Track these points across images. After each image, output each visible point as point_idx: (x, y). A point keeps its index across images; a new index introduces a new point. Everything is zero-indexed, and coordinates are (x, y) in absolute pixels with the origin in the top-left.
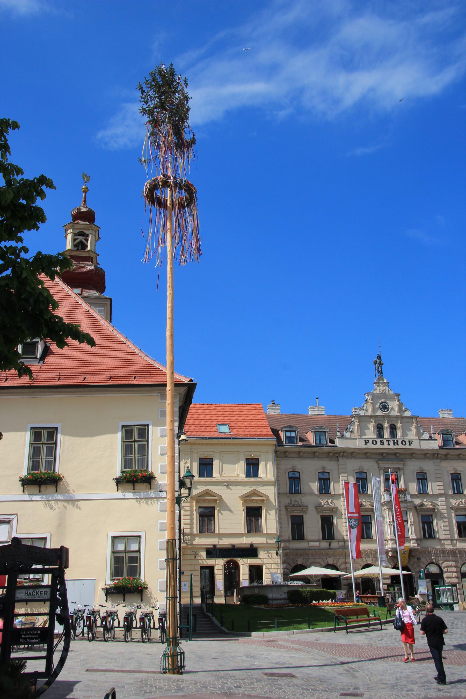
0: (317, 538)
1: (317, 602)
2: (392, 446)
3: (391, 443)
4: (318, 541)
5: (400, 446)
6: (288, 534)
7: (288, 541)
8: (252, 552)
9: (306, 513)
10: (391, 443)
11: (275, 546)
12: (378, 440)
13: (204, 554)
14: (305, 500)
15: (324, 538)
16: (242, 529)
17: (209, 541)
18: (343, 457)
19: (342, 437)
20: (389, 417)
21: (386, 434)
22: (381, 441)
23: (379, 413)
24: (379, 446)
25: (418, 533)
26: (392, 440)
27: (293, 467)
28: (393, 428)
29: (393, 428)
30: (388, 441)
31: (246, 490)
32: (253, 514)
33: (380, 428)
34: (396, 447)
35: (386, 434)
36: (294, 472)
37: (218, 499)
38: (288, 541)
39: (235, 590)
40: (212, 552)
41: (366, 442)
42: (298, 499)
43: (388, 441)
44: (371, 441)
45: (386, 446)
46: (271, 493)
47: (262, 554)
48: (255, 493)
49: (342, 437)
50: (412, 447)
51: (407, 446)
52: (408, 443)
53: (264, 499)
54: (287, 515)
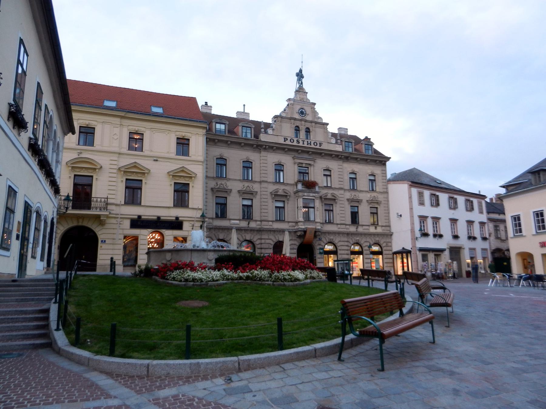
0: (238, 218)
1: (342, 282)
2: (305, 145)
3: (306, 143)
4: (239, 220)
5: (313, 146)
6: (212, 212)
7: (212, 219)
8: (177, 224)
9: (229, 195)
10: (306, 143)
11: (200, 219)
12: (295, 139)
13: (127, 223)
14: (230, 185)
15: (244, 218)
16: (170, 202)
17: (134, 211)
18: (265, 149)
19: (266, 132)
20: (306, 121)
21: (302, 134)
22: (297, 141)
23: (297, 116)
24: (295, 143)
25: (321, 218)
26: (306, 140)
27: (220, 155)
28: (308, 131)
29: (308, 131)
30: (303, 141)
31: (174, 166)
32: (181, 194)
33: (297, 129)
34: (309, 146)
35: (302, 134)
36: (221, 158)
37: (145, 172)
38: (212, 219)
39: (71, 245)
40: (138, 223)
41: (285, 139)
42: (223, 183)
43: (303, 141)
44: (289, 139)
45: (301, 144)
46: (199, 170)
47: (186, 225)
48: (183, 170)
49: (266, 132)
50: (322, 147)
51: (318, 147)
52: (318, 145)
53: (191, 176)
54: (213, 196)
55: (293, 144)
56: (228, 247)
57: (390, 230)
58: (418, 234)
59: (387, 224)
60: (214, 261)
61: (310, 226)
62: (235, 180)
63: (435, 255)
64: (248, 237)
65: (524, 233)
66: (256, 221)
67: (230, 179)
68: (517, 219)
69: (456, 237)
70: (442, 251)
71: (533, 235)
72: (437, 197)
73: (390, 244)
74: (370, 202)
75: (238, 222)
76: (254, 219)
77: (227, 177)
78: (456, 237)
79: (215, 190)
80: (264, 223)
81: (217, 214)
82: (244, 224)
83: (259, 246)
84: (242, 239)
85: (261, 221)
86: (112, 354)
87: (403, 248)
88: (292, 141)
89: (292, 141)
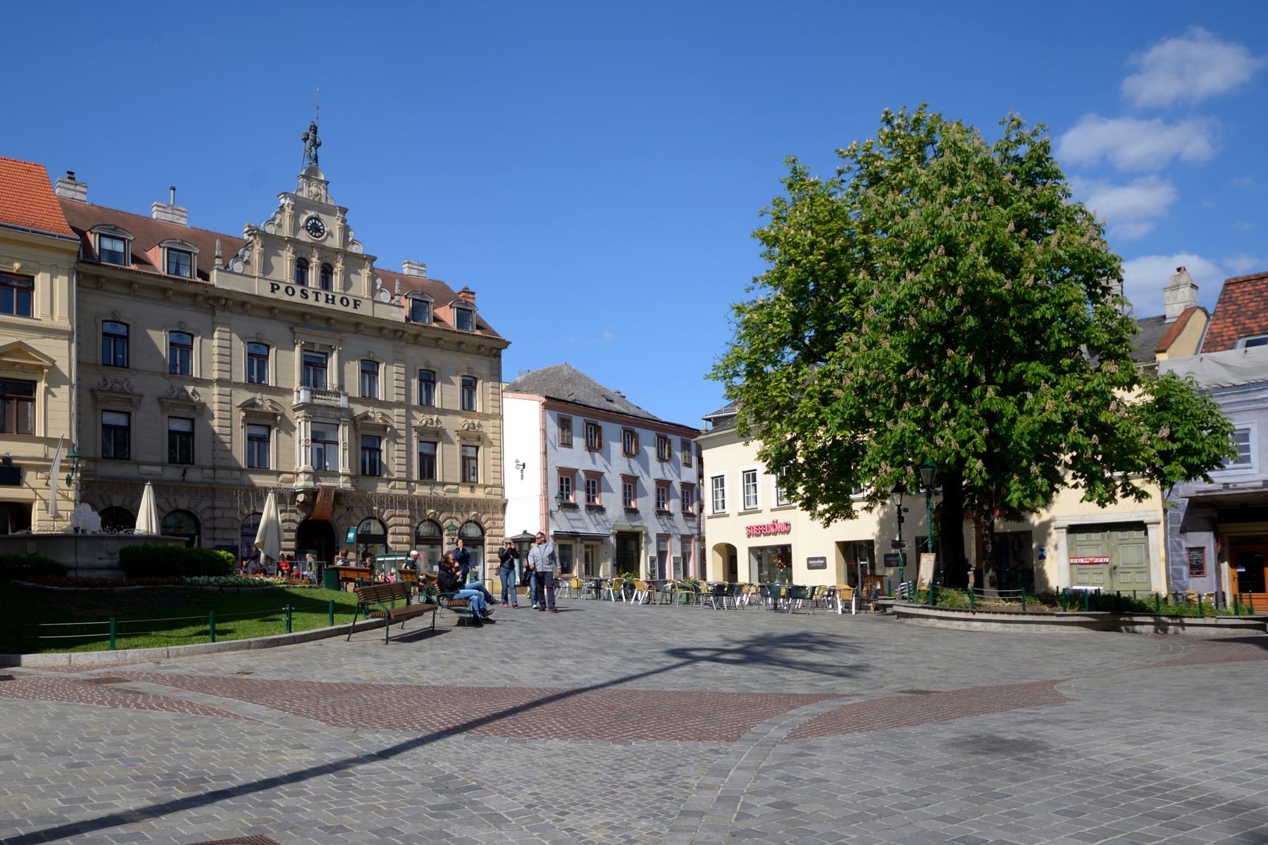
0: (158, 459)
2: (322, 303)
3: (322, 298)
4: (162, 465)
5: (338, 306)
10: (322, 298)
14: (137, 383)
15: (172, 460)
22: (302, 291)
24: (297, 298)
26: (323, 293)
27: (113, 313)
34: (330, 306)
41: (274, 287)
44: (283, 287)
45: (311, 301)
47: (30, 477)
51: (350, 309)
52: (352, 303)
55: (293, 299)
56: (716, 672)
57: (502, 495)
58: (554, 505)
59: (498, 482)
60: (117, 556)
61: (326, 483)
62: (152, 373)
63: (587, 546)
64: (183, 504)
65: (727, 510)
66: (202, 468)
67: (138, 371)
68: (719, 481)
69: (632, 512)
70: (600, 539)
71: (740, 514)
72: (598, 429)
73: (500, 523)
74: (463, 435)
75: (158, 469)
76: (196, 462)
77: (131, 365)
78: (632, 512)
79: (100, 395)
80: (220, 473)
81: (104, 449)
82: (173, 473)
83: (207, 525)
84: (168, 509)
85: (214, 468)
86: (261, 514)
87: (525, 532)
88: (290, 291)
89: (290, 291)
